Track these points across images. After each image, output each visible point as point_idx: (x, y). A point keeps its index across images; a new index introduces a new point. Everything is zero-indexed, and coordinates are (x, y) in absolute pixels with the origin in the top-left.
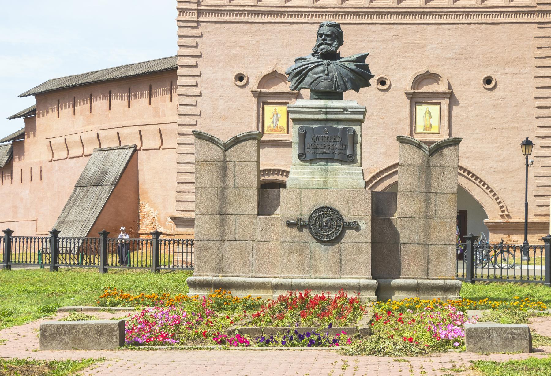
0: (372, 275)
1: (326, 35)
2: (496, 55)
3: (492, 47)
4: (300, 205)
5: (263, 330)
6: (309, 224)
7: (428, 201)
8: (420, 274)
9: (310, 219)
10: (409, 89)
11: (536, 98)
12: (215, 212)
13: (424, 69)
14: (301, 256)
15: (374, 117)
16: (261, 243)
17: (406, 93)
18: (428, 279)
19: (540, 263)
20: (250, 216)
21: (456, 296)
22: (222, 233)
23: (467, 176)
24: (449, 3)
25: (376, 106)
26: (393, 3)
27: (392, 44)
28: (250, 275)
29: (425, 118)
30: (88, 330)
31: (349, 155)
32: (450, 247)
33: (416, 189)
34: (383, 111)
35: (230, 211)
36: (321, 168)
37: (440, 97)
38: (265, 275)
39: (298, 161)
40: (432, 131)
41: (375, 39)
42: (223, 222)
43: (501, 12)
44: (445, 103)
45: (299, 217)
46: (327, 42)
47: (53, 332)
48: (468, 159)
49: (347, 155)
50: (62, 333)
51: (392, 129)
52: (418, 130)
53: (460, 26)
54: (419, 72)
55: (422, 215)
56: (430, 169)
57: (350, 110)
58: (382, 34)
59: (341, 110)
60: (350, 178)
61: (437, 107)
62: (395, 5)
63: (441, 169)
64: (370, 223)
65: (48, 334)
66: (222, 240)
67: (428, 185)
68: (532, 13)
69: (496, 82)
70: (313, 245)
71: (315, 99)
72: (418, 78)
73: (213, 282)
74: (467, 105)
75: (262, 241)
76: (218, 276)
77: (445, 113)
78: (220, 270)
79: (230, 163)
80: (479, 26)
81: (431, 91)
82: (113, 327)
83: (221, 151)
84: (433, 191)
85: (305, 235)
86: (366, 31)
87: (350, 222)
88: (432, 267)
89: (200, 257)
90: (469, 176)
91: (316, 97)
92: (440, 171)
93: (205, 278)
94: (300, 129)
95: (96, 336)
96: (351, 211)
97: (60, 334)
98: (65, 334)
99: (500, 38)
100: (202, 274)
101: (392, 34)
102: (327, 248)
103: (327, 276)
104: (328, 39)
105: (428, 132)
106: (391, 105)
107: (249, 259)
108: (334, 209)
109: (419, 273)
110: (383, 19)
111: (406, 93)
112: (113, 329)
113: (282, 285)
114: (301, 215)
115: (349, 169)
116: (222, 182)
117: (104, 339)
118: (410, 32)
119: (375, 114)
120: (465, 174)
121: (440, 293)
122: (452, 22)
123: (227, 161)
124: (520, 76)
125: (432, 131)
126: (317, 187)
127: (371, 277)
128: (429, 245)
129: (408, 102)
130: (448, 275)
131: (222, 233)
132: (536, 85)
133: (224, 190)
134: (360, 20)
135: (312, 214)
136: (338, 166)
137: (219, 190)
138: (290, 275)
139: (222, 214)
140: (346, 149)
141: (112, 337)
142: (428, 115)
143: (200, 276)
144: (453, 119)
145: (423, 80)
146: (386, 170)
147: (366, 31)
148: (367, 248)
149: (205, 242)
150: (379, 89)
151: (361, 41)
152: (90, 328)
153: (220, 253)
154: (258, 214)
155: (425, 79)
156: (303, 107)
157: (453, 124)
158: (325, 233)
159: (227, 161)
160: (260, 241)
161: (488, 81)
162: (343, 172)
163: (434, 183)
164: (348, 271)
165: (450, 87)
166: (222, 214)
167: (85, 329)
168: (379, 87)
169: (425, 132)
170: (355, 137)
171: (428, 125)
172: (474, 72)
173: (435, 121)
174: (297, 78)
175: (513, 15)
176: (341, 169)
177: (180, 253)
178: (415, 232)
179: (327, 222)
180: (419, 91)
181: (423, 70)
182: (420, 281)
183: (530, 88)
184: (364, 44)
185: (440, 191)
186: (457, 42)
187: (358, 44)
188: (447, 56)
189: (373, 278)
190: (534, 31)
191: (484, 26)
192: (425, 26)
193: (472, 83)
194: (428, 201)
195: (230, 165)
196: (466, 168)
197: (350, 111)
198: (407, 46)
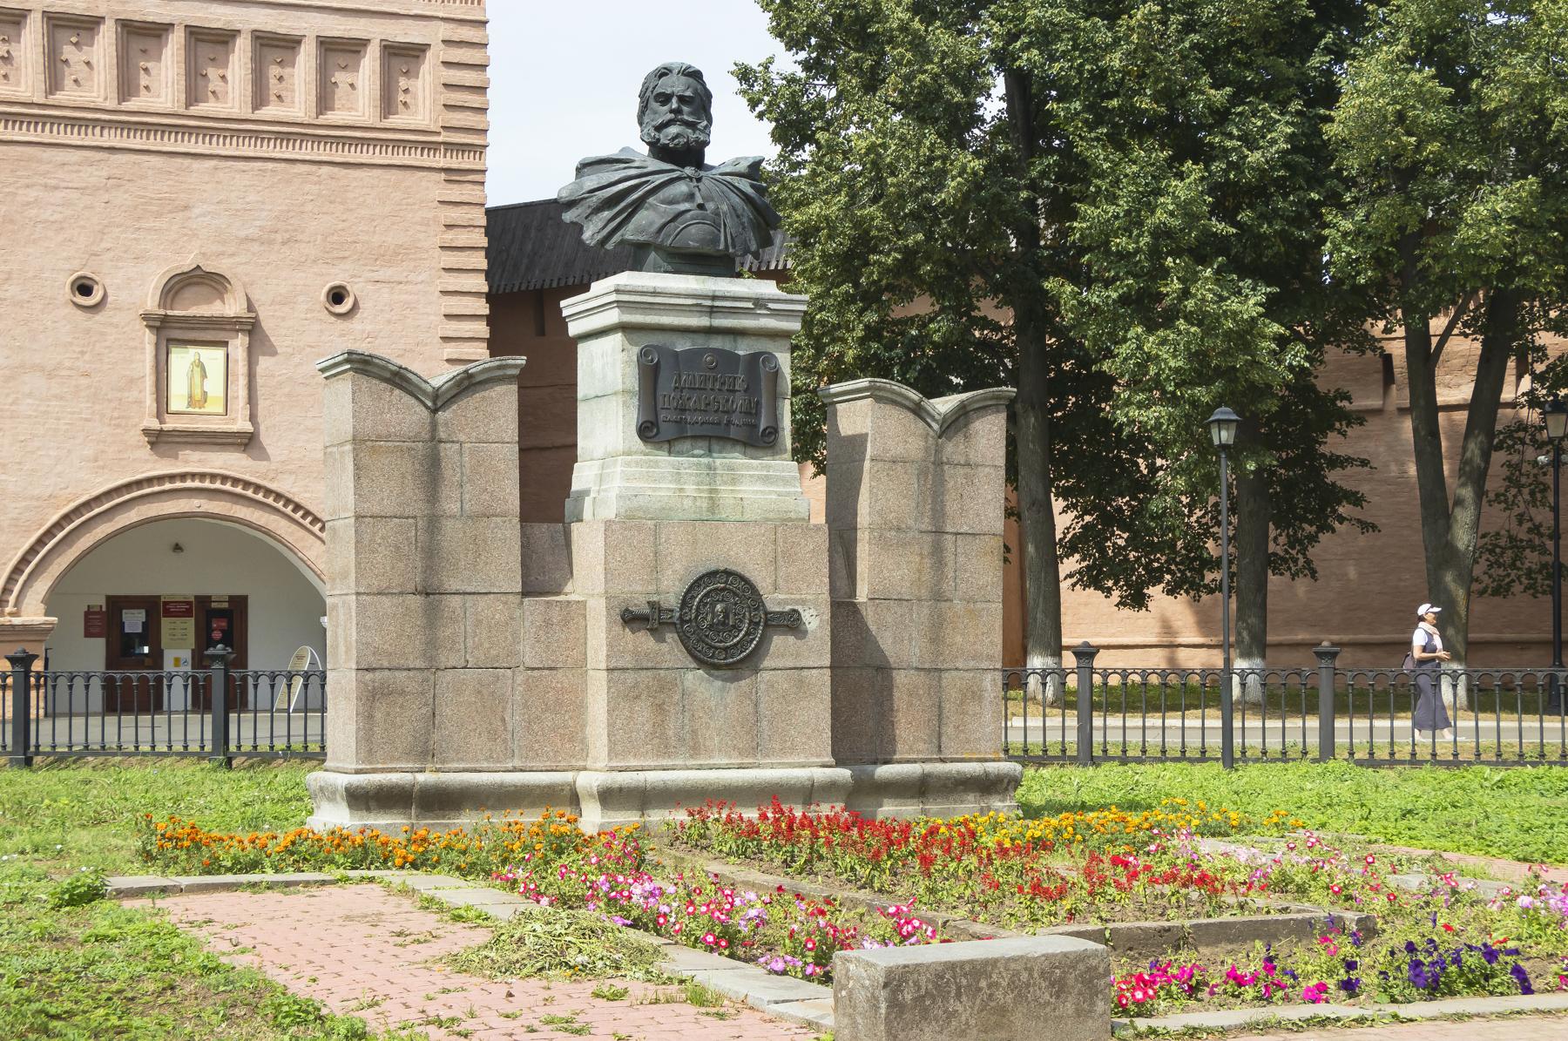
0: (834, 753)
1: (682, 99)
2: (353, 238)
3: (344, 217)
4: (656, 568)
5: (1107, 935)
6: (680, 618)
7: (937, 552)
8: (923, 748)
9: (685, 603)
10: (151, 304)
11: (446, 339)
12: (410, 587)
13: (188, 262)
14: (660, 708)
15: (64, 373)
16: (536, 673)
17: (146, 317)
18: (943, 761)
19: (1022, 711)
20: (503, 598)
21: (1008, 803)
22: (432, 645)
23: (292, 514)
24: (243, 110)
25: (71, 344)
26: (106, 99)
27: (106, 197)
28: (510, 765)
29: (191, 379)
30: (1024, 976)
31: (765, 430)
32: (989, 677)
33: (911, 522)
34: (87, 357)
35: (453, 584)
36: (699, 464)
37: (225, 330)
38: (548, 763)
39: (638, 443)
40: (208, 409)
41: (65, 184)
42: (432, 616)
43: (363, 141)
44: (239, 344)
45: (655, 598)
46: (686, 117)
47: (923, 992)
48: (294, 477)
49: (762, 428)
50: (949, 992)
51: (110, 401)
52: (173, 407)
53: (270, 165)
54: (177, 268)
55: (924, 593)
56: (942, 470)
57: (771, 305)
58: (80, 171)
59: (750, 305)
60: (770, 492)
61: (219, 353)
62: (112, 104)
63: (968, 470)
64: (827, 616)
65: (908, 997)
66: (433, 667)
67: (938, 513)
68: (432, 147)
69: (356, 300)
70: (690, 675)
71: (666, 272)
72: (173, 282)
73: (417, 787)
74: (290, 350)
75: (538, 669)
76: (422, 771)
77: (240, 368)
78: (425, 753)
79: (449, 445)
80: (314, 168)
81: (207, 314)
82: (1094, 962)
83: (425, 413)
84: (949, 529)
85: (670, 650)
86: (40, 161)
87: (782, 613)
88: (949, 730)
89: (371, 717)
90: (298, 516)
91: (670, 268)
92: (966, 476)
93: (394, 778)
94: (643, 354)
95: (1047, 996)
96: (780, 581)
97: (945, 999)
98: (958, 996)
99: (361, 199)
100: (380, 766)
101: (105, 174)
102: (724, 688)
103: (725, 761)
104: (685, 109)
105: (197, 410)
106: (108, 344)
107: (503, 720)
108: (743, 578)
109: (921, 746)
110: (83, 135)
111: (146, 317)
112: (1096, 968)
113: (621, 789)
114: (658, 593)
115: (768, 468)
116: (428, 501)
117: (1069, 1007)
118: (150, 172)
119: (67, 364)
120: (289, 510)
121: (971, 797)
122: (252, 154)
123: (440, 441)
124: (409, 287)
125: (208, 409)
126: (694, 516)
127: (832, 761)
128: (941, 670)
129: (149, 338)
130: (988, 747)
131: (432, 645)
132: (444, 311)
133: (433, 523)
134: (24, 135)
135: (689, 591)
136: (737, 460)
137: (420, 523)
138: (633, 763)
139: (429, 592)
140: (757, 414)
141: (1092, 998)
142: (197, 370)
143: (374, 771)
144: (260, 381)
145: (182, 288)
146: (98, 499)
147: (40, 161)
148: (822, 680)
149: (387, 673)
150: (76, 304)
151: (28, 186)
152: (1030, 970)
153: (426, 704)
154: (525, 593)
155: (189, 284)
156: (655, 293)
157: (261, 391)
158: (721, 642)
159: (440, 441)
160: (533, 669)
161: (337, 296)
162: (751, 476)
163: (952, 507)
164: (777, 747)
165: (250, 308)
166: (429, 592)
167: (1017, 974)
168: (75, 299)
169: (190, 410)
170: (779, 380)
171: (198, 395)
172: (304, 275)
173: (215, 386)
174: (607, 214)
175: (390, 149)
176: (749, 467)
177: (265, 711)
178: (910, 640)
179: (726, 613)
180: (176, 313)
181: (187, 264)
182: (929, 768)
183: (432, 318)
184: (35, 194)
185: (965, 529)
186: (263, 203)
187: (20, 192)
188: (242, 234)
189: (840, 762)
190: (435, 187)
191: (325, 169)
192: (187, 161)
193: (301, 299)
194: (937, 552)
195: (448, 451)
196: (290, 496)
197: (770, 309)
198: (142, 204)
